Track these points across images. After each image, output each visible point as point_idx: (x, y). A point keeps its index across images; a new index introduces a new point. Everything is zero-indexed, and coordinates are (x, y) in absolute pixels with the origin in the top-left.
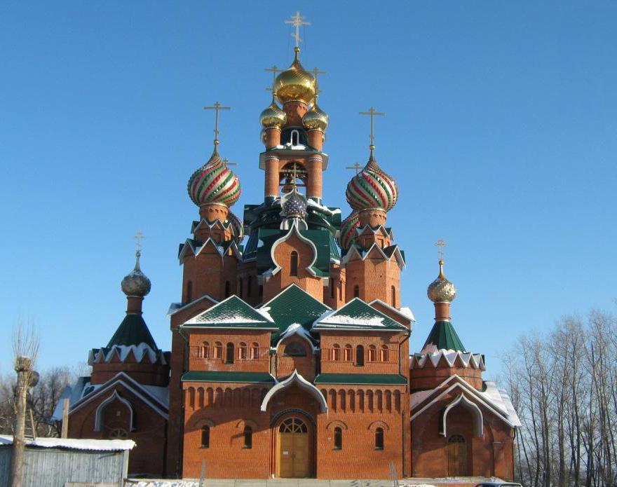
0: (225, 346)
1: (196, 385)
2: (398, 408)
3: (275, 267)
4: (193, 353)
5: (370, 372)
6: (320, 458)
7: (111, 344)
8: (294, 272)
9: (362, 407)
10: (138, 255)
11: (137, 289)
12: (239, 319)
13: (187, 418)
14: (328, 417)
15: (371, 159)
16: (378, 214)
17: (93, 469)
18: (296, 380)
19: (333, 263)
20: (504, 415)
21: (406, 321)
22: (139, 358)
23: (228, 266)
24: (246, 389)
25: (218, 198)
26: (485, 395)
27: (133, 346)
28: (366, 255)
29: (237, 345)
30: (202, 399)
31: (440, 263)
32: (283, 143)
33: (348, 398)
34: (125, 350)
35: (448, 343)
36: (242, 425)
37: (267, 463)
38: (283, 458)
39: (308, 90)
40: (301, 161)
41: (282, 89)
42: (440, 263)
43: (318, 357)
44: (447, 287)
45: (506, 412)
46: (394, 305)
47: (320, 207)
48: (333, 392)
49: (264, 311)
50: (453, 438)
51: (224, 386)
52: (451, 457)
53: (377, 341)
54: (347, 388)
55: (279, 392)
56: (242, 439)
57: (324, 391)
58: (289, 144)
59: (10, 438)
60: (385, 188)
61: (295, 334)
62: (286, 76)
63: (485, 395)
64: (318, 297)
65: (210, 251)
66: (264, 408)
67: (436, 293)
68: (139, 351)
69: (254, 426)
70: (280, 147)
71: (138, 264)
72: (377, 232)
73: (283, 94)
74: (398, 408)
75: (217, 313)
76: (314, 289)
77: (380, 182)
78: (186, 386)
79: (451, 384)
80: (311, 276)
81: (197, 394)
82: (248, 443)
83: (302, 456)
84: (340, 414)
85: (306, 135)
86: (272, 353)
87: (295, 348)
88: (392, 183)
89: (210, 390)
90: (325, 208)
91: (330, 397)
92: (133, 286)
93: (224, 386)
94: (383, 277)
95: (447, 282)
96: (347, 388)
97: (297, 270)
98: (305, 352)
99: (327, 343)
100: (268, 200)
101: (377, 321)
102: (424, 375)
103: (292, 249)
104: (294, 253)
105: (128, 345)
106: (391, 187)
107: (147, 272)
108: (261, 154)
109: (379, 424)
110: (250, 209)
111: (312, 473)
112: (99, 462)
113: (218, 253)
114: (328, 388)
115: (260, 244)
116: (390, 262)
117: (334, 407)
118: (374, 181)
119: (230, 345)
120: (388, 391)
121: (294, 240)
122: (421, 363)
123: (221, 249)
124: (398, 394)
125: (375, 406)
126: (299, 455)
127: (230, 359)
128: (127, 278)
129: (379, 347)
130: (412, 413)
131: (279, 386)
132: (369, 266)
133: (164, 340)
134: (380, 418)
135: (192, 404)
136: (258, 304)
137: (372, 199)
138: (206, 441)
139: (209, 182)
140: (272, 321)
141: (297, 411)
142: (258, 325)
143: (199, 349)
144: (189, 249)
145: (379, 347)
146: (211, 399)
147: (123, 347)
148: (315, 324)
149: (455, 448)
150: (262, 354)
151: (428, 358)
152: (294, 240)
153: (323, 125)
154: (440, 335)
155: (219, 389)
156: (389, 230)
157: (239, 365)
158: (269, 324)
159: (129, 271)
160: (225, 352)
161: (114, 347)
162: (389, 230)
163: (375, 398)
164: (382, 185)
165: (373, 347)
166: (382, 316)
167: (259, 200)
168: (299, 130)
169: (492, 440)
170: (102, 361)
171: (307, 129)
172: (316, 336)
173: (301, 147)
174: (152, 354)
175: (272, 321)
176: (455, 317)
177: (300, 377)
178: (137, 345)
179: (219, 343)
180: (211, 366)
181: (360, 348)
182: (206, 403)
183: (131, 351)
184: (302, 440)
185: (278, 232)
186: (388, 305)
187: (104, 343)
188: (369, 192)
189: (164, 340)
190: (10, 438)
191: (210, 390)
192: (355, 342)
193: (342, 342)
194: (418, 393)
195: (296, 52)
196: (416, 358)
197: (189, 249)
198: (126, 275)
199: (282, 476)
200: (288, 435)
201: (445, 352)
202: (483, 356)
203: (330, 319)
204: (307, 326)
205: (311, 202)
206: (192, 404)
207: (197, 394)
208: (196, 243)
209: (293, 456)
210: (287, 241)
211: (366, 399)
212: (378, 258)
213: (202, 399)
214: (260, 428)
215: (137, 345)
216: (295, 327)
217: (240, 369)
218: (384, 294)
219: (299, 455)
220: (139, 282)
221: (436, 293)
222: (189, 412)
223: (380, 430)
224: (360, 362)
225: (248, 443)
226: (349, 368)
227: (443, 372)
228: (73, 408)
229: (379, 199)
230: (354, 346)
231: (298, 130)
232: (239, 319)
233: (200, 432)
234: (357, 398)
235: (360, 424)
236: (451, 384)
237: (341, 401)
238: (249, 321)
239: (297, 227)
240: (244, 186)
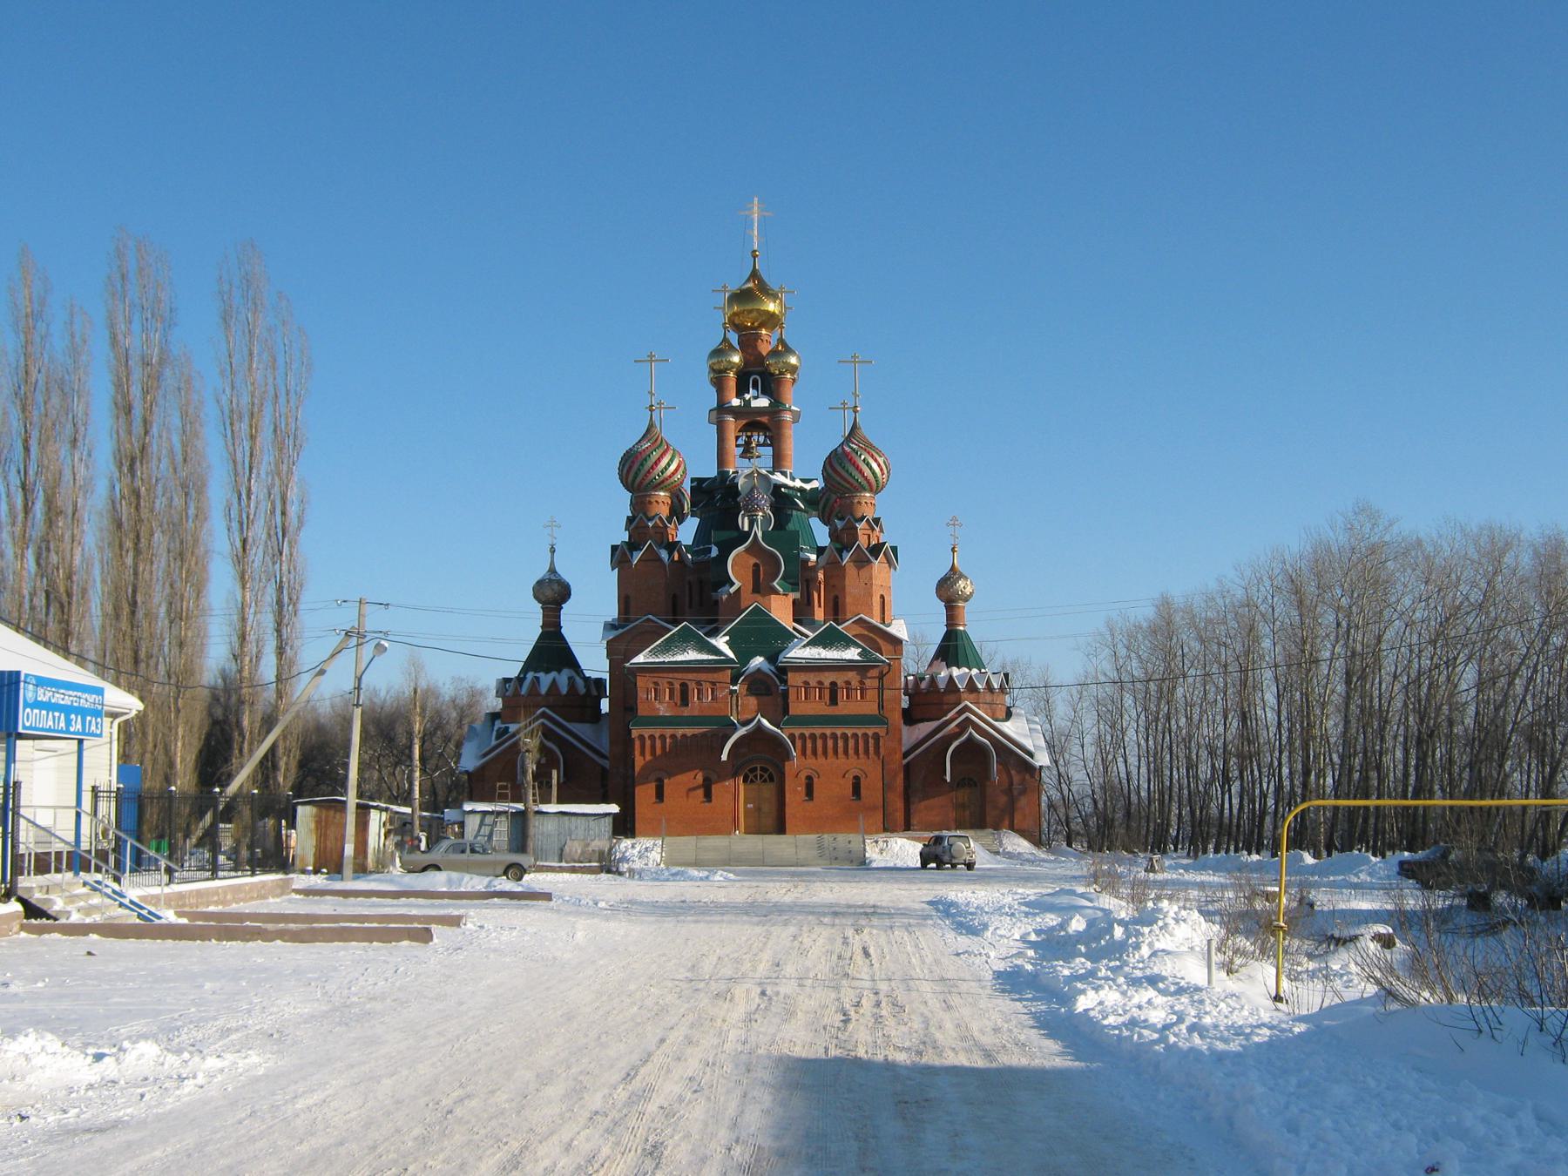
0: (677, 686)
1: (647, 732)
2: (877, 752)
3: (732, 584)
4: (641, 695)
5: (845, 712)
6: (789, 811)
7: (525, 670)
8: (757, 589)
9: (836, 752)
10: (553, 551)
11: (553, 594)
12: (692, 655)
13: (637, 769)
14: (796, 763)
15: (855, 427)
17: (588, 829)
18: (760, 726)
19: (808, 560)
20: (1031, 755)
21: (896, 642)
22: (564, 690)
23: (671, 584)
24: (704, 735)
25: (659, 486)
26: (1008, 727)
27: (554, 674)
28: (847, 557)
29: (692, 685)
30: (653, 747)
31: (953, 550)
32: (739, 395)
33: (819, 743)
34: (546, 679)
35: (960, 657)
36: (700, 778)
37: (730, 819)
38: (747, 811)
39: (772, 315)
40: (765, 419)
41: (735, 314)
42: (953, 550)
43: (785, 694)
44: (961, 583)
45: (1032, 748)
46: (883, 622)
47: (791, 484)
48: (802, 736)
49: (721, 642)
50: (960, 782)
51: (680, 732)
52: (961, 806)
53: (853, 677)
54: (818, 731)
55: (743, 737)
56: (701, 792)
57: (792, 737)
58: (747, 396)
59: (520, 806)
61: (759, 670)
62: (742, 296)
63: (1008, 727)
64: (787, 622)
65: (652, 557)
66: (724, 757)
67: (948, 591)
68: (563, 678)
69: (714, 777)
70: (736, 402)
71: (552, 563)
72: (860, 526)
74: (877, 752)
75: (666, 648)
76: (781, 609)
78: (635, 734)
79: (960, 713)
80: (777, 593)
81: (648, 743)
82: (708, 796)
83: (769, 808)
84: (811, 761)
85: (771, 384)
86: (732, 692)
87: (758, 685)
88: (881, 460)
89: (663, 737)
90: (798, 484)
91: (799, 743)
92: (549, 593)
93: (680, 732)
94: (868, 585)
95: (961, 576)
96: (818, 731)
97: (761, 587)
98: (771, 689)
99: (794, 679)
100: (723, 474)
101: (852, 654)
102: (928, 701)
103: (753, 560)
104: (756, 565)
105: (547, 671)
107: (565, 573)
109: (856, 772)
110: (699, 485)
111: (781, 829)
112: (592, 823)
113: (660, 560)
114: (797, 733)
115: (715, 552)
116: (878, 564)
117: (804, 753)
119: (684, 686)
120: (865, 735)
121: (755, 549)
122: (923, 685)
123: (664, 554)
124: (876, 737)
125: (851, 752)
126: (766, 808)
127: (685, 700)
128: (540, 583)
129: (855, 683)
130: (906, 755)
131: (742, 731)
132: (851, 571)
133: (594, 662)
134: (854, 765)
135: (643, 753)
136: (714, 633)
138: (660, 795)
139: (649, 464)
140: (732, 655)
141: (762, 760)
142: (716, 661)
143: (648, 691)
144: (624, 553)
145: (855, 683)
146: (664, 747)
147: (541, 675)
148: (781, 658)
149: (963, 795)
150: (720, 694)
151: (933, 680)
152: (755, 549)
153: (793, 370)
154: (952, 648)
155: (673, 736)
156: (877, 521)
157: (695, 706)
158: (730, 661)
159: (541, 572)
160: (677, 694)
161: (530, 675)
162: (877, 521)
163: (851, 743)
164: (868, 464)
165: (848, 683)
166: (858, 646)
167: (712, 472)
168: (761, 374)
169: (1011, 784)
170: (517, 693)
171: (773, 375)
172: (782, 672)
173: (763, 402)
174: (580, 682)
175: (732, 655)
176: (973, 625)
177: (765, 722)
178: (559, 671)
179: (671, 684)
180: (663, 710)
181: (833, 684)
182: (658, 752)
183: (554, 682)
184: (768, 790)
185: (735, 534)
186: (876, 621)
187: (513, 671)
189: (594, 662)
190: (520, 806)
191: (663, 737)
192: (827, 678)
193: (813, 679)
194: (921, 725)
196: (919, 679)
197: (624, 553)
198: (539, 577)
199: (747, 832)
200: (753, 786)
201: (956, 672)
202: (1006, 675)
203: (799, 652)
204: (772, 659)
205: (778, 478)
206: (643, 753)
207: (648, 743)
208: (632, 545)
209: (758, 809)
210: (747, 550)
211: (840, 743)
212: (862, 562)
213: (653, 747)
214: (722, 778)
215: (559, 671)
216: (758, 661)
217: (696, 713)
218: (870, 607)
219: (766, 808)
220: (556, 587)
221: (948, 591)
222: (639, 762)
223: (856, 778)
224: (834, 700)
225: (708, 796)
226: (818, 707)
227: (951, 698)
228: (485, 755)
230: (827, 684)
231: (759, 374)
232: (692, 655)
233: (653, 785)
234: (830, 743)
235: (835, 773)
236: (960, 713)
237: (811, 747)
238: (705, 657)
239: (760, 534)
240: (692, 455)
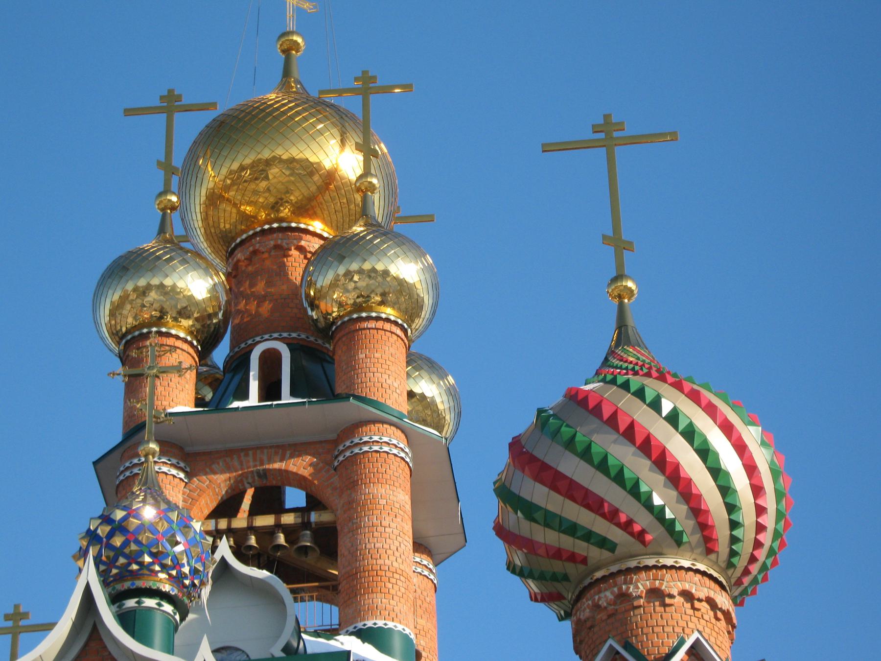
16: (672, 585)
60: (705, 452)
73: (227, 219)
77: (673, 419)
88: (752, 435)
106: (741, 448)
108: (95, 463)
118: (642, 415)
137: (629, 508)
164: (690, 434)
188: (603, 466)
195: (286, 52)
229: (676, 513)
